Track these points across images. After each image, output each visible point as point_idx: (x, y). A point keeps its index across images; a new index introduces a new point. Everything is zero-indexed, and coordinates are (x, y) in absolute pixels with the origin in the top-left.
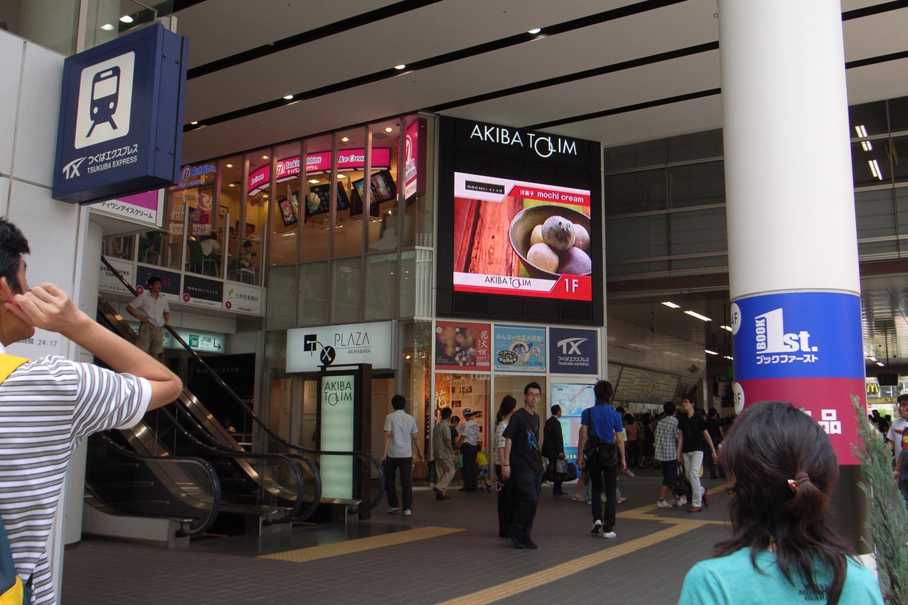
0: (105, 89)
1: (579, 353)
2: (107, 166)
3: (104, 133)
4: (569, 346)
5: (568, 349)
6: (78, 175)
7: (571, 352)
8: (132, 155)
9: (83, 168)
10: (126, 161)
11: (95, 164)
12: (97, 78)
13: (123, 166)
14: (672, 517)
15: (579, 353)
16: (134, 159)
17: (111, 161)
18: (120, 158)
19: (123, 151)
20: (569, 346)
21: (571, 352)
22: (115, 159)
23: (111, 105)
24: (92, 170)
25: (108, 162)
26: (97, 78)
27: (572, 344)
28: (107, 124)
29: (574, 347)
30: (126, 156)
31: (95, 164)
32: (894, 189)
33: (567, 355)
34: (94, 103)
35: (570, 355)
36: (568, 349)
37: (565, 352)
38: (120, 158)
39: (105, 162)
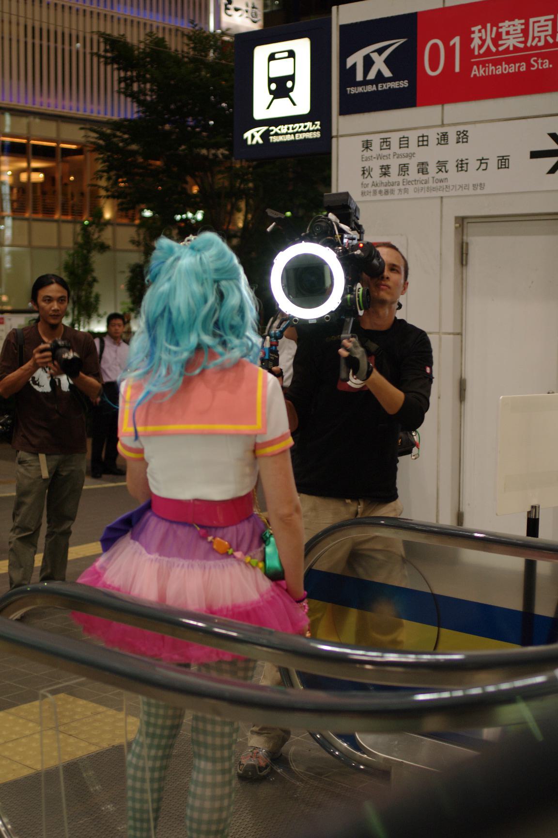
0: (281, 68)
1: (387, 73)
2: (291, 138)
3: (282, 108)
4: (368, 62)
5: (366, 71)
6: (261, 142)
7: (372, 75)
8: (313, 131)
9: (265, 136)
10: (309, 135)
11: (276, 134)
12: (272, 57)
13: (306, 140)
14: (522, 679)
15: (387, 73)
16: (318, 135)
17: (294, 134)
18: (302, 132)
19: (305, 127)
20: (368, 62)
21: (372, 75)
22: (297, 132)
23: (289, 84)
24: (274, 139)
25: (291, 134)
26: (272, 57)
27: (375, 56)
28: (286, 100)
29: (380, 64)
30: (308, 131)
31: (276, 134)
32: (435, 651)
33: (365, 82)
34: (271, 81)
35: (371, 82)
36: (366, 71)
37: (359, 77)
38: (302, 132)
39: (287, 134)
